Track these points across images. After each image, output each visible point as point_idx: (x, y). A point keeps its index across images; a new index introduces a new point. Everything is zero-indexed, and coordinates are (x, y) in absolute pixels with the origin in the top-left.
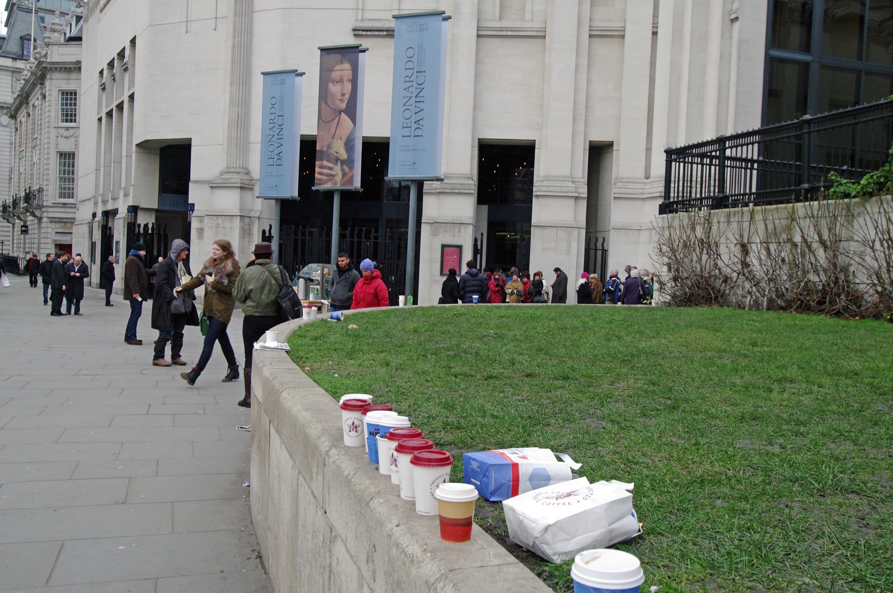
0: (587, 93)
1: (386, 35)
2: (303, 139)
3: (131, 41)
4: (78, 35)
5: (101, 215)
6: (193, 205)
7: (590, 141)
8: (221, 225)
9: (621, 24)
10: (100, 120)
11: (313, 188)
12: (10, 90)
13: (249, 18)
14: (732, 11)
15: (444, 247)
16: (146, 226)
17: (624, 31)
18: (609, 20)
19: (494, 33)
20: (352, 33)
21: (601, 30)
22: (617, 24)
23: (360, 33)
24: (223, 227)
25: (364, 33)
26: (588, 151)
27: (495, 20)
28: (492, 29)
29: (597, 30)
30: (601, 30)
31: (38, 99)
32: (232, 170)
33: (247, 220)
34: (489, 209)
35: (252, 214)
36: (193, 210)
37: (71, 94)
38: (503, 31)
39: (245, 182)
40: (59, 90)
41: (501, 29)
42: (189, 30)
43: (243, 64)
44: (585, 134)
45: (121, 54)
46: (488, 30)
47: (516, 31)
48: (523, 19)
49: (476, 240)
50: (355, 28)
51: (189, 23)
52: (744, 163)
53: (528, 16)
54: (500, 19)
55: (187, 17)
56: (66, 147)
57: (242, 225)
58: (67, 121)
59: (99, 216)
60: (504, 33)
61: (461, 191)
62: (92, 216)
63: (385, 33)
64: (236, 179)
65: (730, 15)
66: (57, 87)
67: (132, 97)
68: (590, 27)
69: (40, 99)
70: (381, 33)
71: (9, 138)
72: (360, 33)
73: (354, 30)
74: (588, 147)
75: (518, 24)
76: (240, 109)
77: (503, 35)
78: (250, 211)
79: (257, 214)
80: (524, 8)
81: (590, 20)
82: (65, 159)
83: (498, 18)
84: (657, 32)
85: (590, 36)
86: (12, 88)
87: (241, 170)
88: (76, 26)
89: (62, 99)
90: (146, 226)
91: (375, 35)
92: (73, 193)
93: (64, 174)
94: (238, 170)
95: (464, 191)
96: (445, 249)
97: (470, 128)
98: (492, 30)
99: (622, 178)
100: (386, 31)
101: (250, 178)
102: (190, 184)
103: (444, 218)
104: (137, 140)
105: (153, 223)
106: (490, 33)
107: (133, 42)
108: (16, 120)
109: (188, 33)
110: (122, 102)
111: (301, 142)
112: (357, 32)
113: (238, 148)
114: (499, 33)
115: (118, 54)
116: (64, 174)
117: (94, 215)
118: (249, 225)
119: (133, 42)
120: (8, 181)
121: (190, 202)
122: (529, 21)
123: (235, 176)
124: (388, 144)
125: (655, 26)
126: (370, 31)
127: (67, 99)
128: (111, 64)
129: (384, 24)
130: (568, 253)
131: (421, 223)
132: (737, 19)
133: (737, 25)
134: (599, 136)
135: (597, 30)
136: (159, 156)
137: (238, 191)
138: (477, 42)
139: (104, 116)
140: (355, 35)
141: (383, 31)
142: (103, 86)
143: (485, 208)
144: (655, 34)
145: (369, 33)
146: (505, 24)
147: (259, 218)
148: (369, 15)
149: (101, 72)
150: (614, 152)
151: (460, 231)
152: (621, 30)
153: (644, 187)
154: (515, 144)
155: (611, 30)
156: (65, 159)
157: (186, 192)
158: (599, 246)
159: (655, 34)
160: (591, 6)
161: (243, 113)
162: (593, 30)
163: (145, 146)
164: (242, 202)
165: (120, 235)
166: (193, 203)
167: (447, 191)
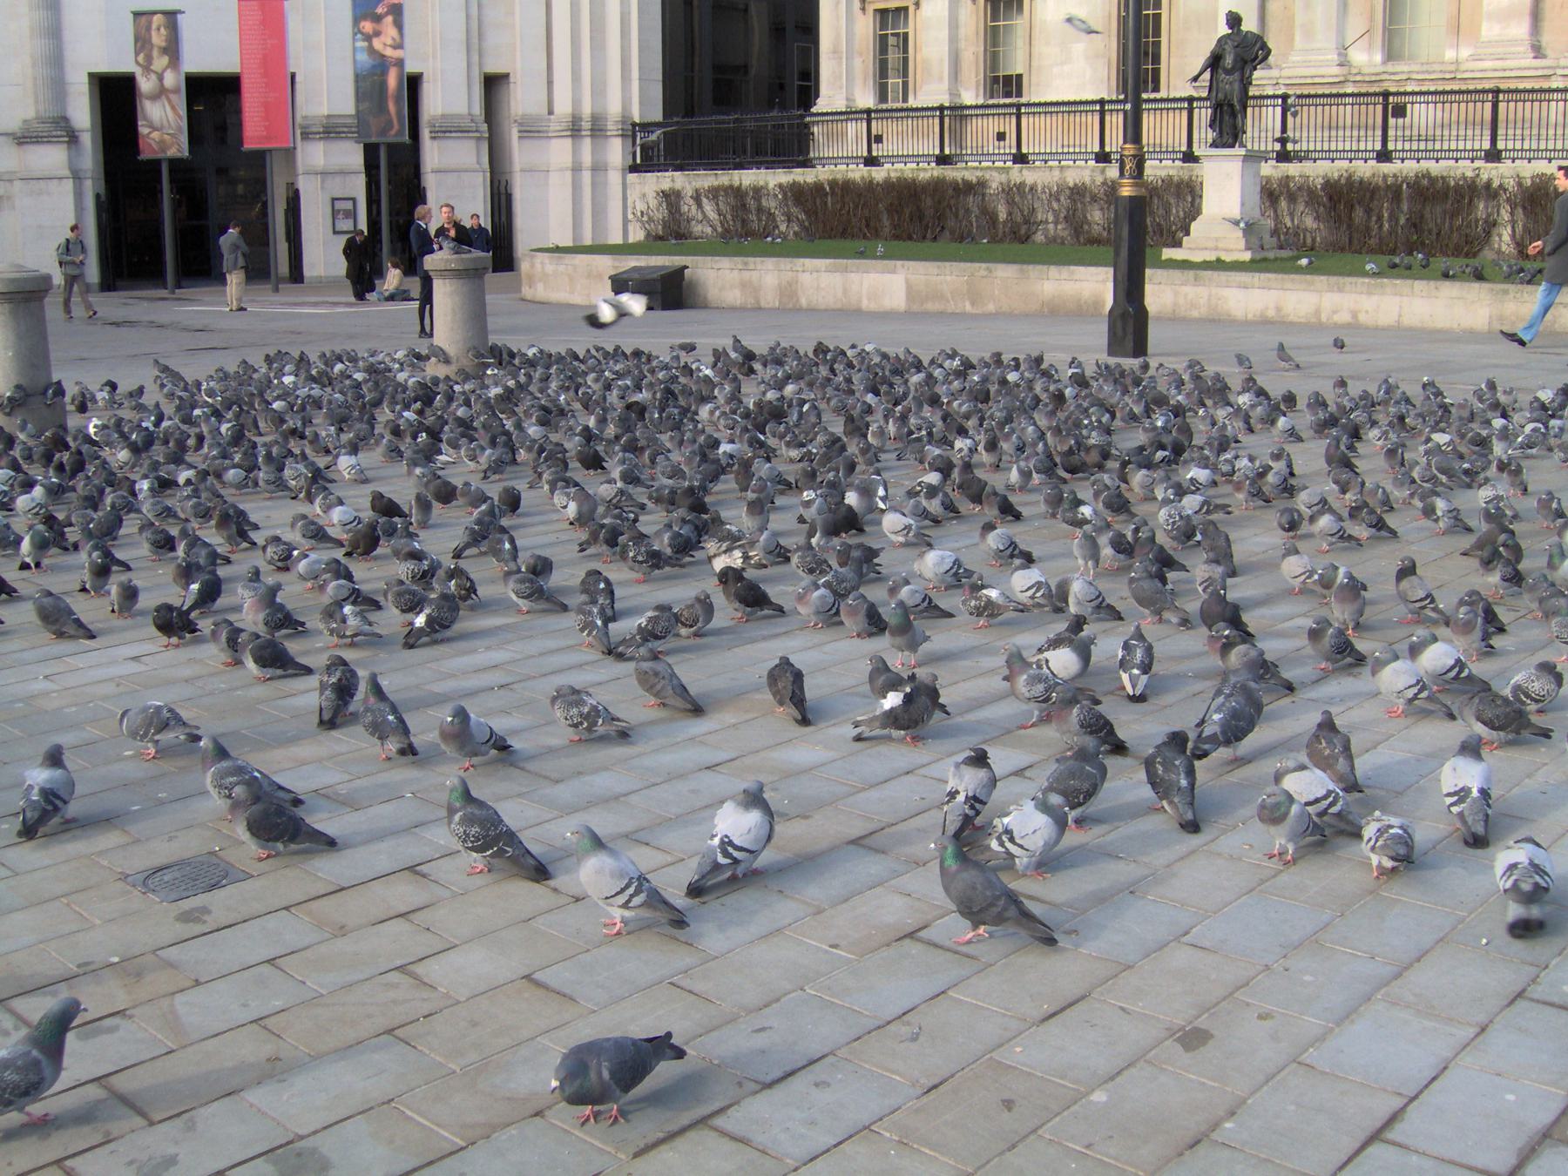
134: (493, 68)
150: (512, 85)
158: (502, 190)
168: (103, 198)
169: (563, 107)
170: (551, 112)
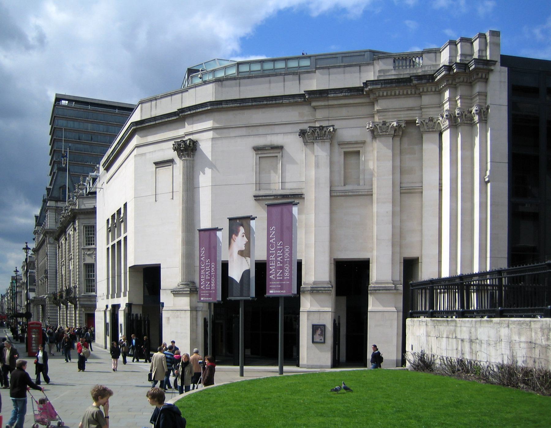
0: (401, 228)
3: (124, 205)
4: (94, 191)
5: (111, 307)
7: (404, 258)
10: (108, 249)
11: (227, 299)
12: (55, 221)
16: (137, 315)
20: (254, 198)
24: (180, 317)
26: (403, 264)
27: (341, 186)
31: (72, 230)
34: (347, 301)
37: (91, 227)
38: (346, 192)
40: (84, 226)
41: (345, 191)
42: (157, 200)
44: (400, 253)
45: (119, 211)
47: (355, 192)
48: (359, 184)
49: (335, 321)
52: (475, 287)
53: (362, 182)
54: (345, 185)
56: (89, 260)
58: (89, 245)
59: (110, 307)
62: (105, 307)
63: (273, 197)
66: (83, 224)
67: (125, 238)
68: (400, 187)
69: (73, 230)
71: (54, 251)
74: (420, 264)
75: (356, 187)
77: (346, 195)
80: (359, 178)
81: (400, 183)
82: (89, 268)
83: (343, 185)
85: (401, 193)
86: (56, 219)
88: (93, 185)
89: (86, 241)
90: (137, 315)
92: (94, 275)
93: (89, 277)
102: (161, 290)
104: (129, 265)
105: (141, 314)
107: (125, 205)
108: (59, 242)
110: (120, 240)
115: (117, 211)
116: (89, 277)
117: (107, 306)
119: (125, 205)
120: (55, 273)
121: (161, 302)
122: (362, 185)
127: (89, 231)
128: (113, 216)
129: (273, 192)
131: (300, 312)
134: (411, 254)
135: (405, 189)
136: (143, 273)
139: (110, 247)
140: (255, 199)
142: (109, 229)
143: (343, 299)
146: (348, 187)
149: (108, 220)
156: (89, 268)
160: (400, 175)
163: (134, 268)
165: (121, 319)
166: (163, 302)
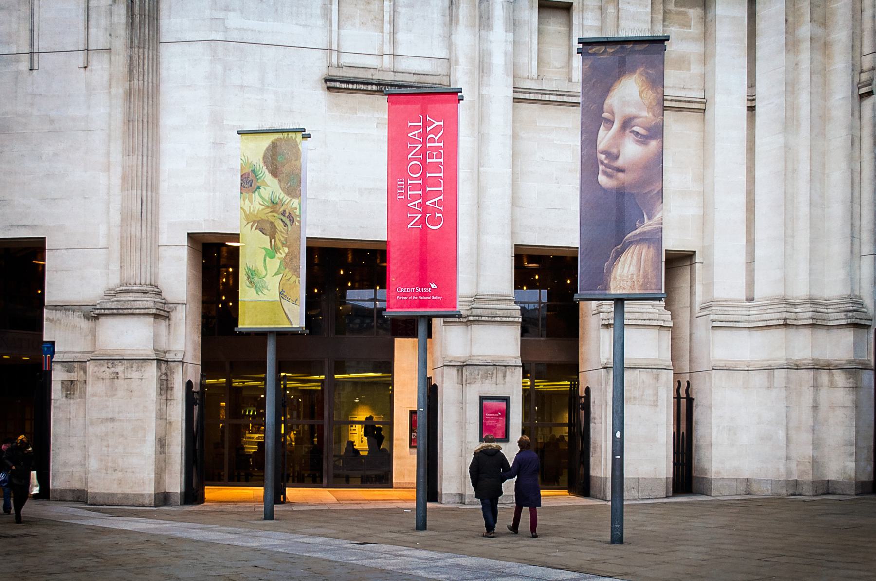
1: (377, 91)
2: (311, 245)
6: (53, 343)
8: (121, 375)
9: (701, 95)
13: (155, 52)
14: (860, 83)
15: (482, 399)
17: (705, 103)
18: (684, 88)
19: (532, 97)
21: (676, 101)
22: (695, 94)
23: (338, 85)
25: (344, 86)
28: (530, 91)
29: (671, 100)
30: (676, 101)
32: (135, 288)
33: (163, 366)
35: (170, 357)
36: (53, 352)
39: (159, 306)
41: (543, 92)
43: (148, 122)
46: (525, 92)
47: (563, 95)
50: (328, 77)
51: (35, 56)
55: (32, 45)
57: (160, 373)
60: (547, 98)
61: (504, 319)
63: (374, 88)
64: (148, 302)
65: (859, 88)
70: (370, 87)
72: (338, 85)
73: (326, 81)
76: (144, 192)
78: (165, 352)
79: (179, 357)
84: (755, 106)
87: (149, 288)
91: (360, 90)
94: (144, 288)
95: (507, 319)
96: (485, 402)
97: (507, 230)
98: (530, 93)
99: (718, 301)
100: (377, 84)
101: (163, 301)
103: (480, 358)
106: (527, 96)
109: (35, 72)
111: (310, 251)
112: (333, 84)
113: (144, 253)
114: (539, 97)
118: (166, 374)
123: (140, 297)
124: (575, 259)
125: (752, 99)
126: (353, 83)
130: (655, 404)
132: (870, 94)
133: (868, 103)
135: (671, 100)
137: (151, 319)
138: (514, 108)
140: (328, 88)
141: (372, 84)
144: (751, 109)
145: (350, 86)
147: (183, 363)
148: (346, 60)
151: (504, 377)
152: (701, 103)
153: (748, 313)
154: (536, 254)
155: (689, 102)
157: (37, 325)
159: (751, 109)
161: (149, 199)
162: (666, 100)
164: (156, 337)
167: (483, 319)
168: (196, 388)
169: (764, 289)
170: (751, 299)
